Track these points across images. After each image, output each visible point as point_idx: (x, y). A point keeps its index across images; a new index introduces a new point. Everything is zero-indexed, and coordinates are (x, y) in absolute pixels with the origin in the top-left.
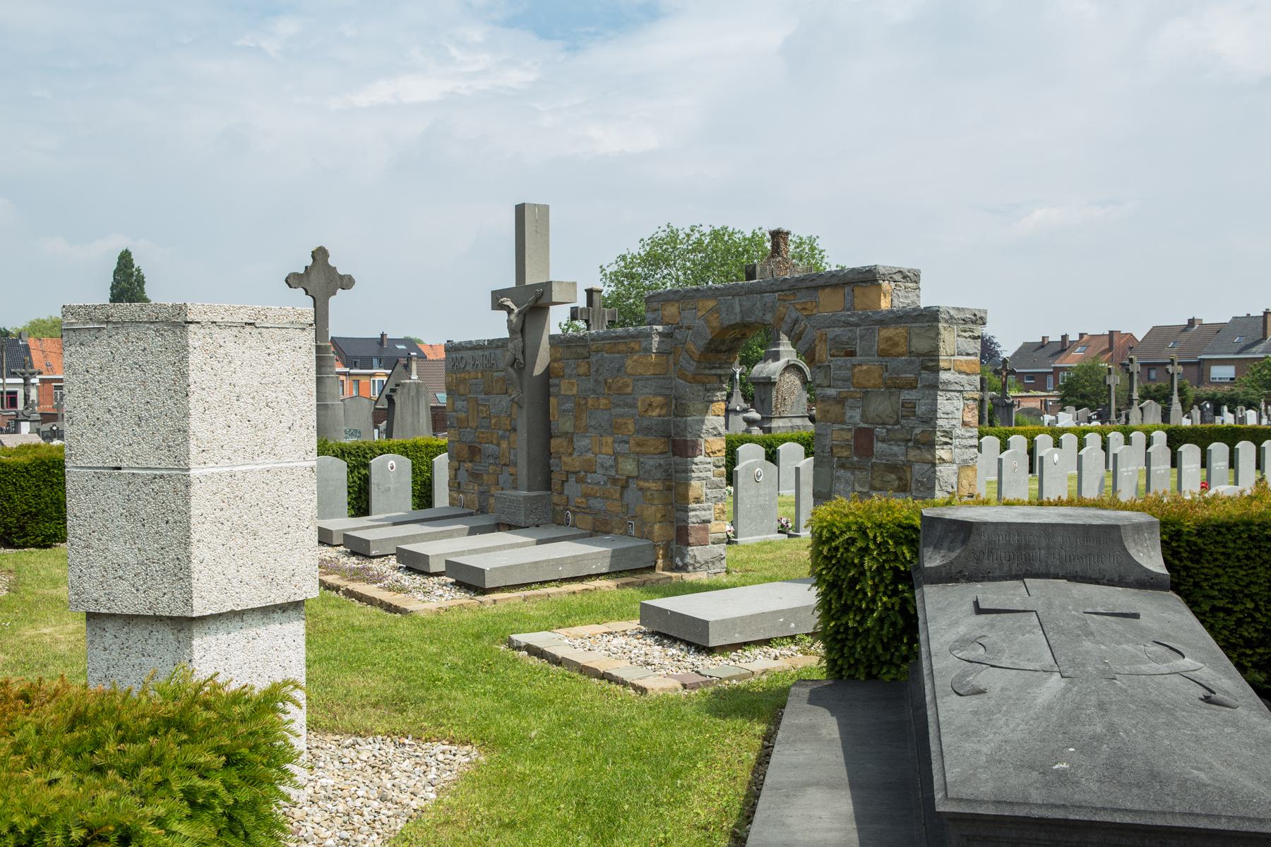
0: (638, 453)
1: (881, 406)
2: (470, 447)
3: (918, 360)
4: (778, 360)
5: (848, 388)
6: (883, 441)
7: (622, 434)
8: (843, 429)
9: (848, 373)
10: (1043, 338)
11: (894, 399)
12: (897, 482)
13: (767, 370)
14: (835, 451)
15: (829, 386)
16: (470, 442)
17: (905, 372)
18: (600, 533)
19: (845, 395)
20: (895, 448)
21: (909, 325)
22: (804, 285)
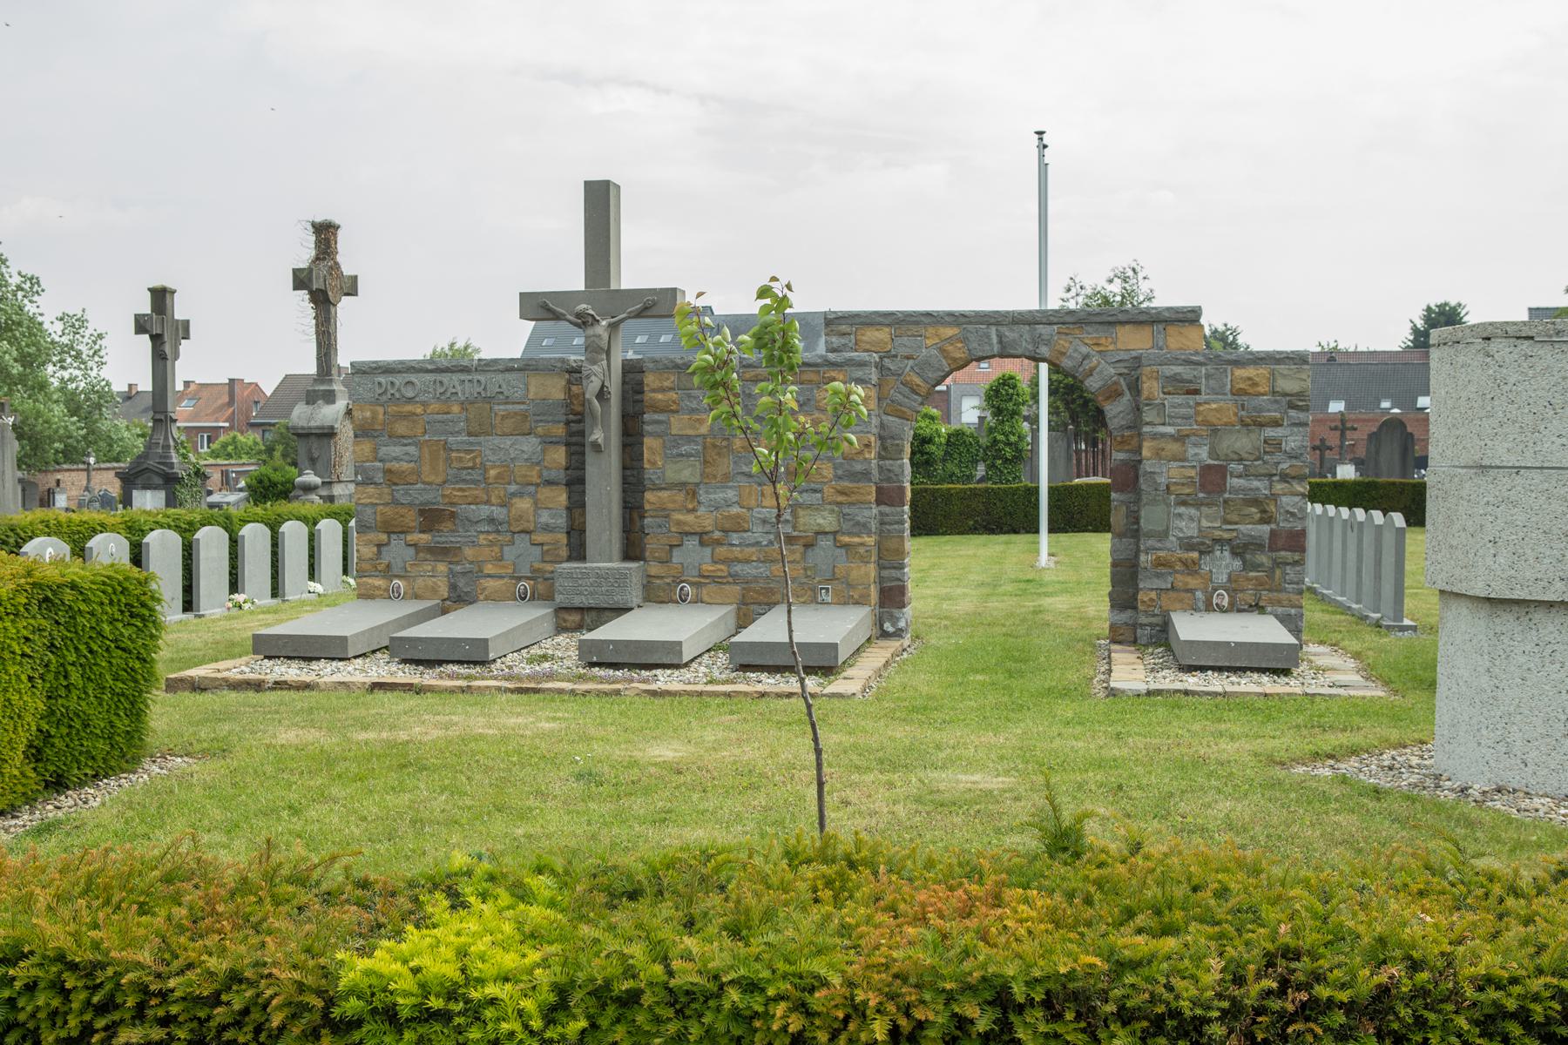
0: (839, 504)
1: (1243, 443)
2: (422, 512)
3: (1284, 400)
4: (333, 402)
6: (1239, 477)
9: (1191, 411)
10: (130, 386)
11: (1253, 436)
15: (1164, 424)
16: (421, 504)
17: (1269, 411)
18: (607, 613)
20: (1256, 484)
22: (1098, 319)
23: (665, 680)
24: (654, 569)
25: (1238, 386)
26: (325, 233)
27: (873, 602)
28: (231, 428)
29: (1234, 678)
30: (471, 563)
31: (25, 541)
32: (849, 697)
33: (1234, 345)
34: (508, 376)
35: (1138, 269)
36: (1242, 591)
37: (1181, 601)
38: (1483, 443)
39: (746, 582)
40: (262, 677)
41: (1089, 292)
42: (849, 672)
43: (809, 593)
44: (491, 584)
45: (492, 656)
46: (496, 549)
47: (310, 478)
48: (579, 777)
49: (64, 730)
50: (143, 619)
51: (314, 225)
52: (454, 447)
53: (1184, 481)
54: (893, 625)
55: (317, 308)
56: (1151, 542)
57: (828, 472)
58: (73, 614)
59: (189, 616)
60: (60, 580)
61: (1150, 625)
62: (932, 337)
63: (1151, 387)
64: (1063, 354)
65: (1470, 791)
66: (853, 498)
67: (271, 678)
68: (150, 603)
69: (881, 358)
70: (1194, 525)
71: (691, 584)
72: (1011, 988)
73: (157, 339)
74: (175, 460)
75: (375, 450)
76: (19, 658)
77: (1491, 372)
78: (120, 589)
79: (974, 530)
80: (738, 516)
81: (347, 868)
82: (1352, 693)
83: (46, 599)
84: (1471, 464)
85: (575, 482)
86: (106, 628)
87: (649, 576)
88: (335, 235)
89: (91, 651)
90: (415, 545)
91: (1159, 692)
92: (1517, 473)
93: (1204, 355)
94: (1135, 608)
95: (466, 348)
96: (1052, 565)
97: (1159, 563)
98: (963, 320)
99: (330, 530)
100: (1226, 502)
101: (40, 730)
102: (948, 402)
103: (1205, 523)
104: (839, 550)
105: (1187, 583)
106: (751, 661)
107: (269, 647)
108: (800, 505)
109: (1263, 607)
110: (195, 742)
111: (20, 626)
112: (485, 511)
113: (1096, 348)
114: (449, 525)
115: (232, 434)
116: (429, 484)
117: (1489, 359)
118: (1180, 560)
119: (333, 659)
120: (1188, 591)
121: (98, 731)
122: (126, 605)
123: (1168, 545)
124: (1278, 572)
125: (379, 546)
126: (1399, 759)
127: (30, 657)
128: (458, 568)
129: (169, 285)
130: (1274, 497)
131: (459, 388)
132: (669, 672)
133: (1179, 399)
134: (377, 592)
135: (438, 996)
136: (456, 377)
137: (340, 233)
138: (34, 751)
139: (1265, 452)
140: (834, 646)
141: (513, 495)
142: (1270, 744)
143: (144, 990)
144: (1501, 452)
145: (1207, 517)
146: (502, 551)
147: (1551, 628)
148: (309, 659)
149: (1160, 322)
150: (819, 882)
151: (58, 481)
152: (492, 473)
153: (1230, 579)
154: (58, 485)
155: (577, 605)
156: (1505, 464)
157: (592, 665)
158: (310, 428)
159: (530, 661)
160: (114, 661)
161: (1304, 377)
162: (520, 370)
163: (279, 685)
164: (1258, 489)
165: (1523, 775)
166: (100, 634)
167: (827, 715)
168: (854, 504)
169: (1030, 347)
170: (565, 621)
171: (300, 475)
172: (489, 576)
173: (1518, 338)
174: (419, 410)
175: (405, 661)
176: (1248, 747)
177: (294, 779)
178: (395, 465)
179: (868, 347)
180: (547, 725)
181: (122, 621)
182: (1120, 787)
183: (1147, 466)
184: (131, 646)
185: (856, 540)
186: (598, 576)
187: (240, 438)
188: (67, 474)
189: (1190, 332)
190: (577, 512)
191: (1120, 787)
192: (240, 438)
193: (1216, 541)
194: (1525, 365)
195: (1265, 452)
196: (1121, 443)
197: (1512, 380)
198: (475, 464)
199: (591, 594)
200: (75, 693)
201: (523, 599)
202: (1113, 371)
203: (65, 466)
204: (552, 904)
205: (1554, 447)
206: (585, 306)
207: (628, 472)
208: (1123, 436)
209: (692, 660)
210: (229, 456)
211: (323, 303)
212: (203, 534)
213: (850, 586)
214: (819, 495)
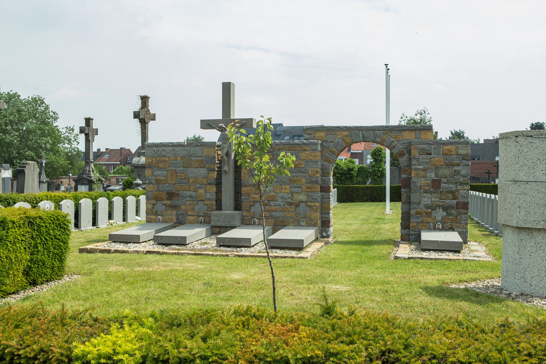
0: (307, 192)
1: (446, 172)
2: (168, 193)
5: (428, 165)
6: (445, 183)
7: (297, 184)
8: (426, 180)
9: (429, 161)
12: (452, 197)
15: (419, 165)
16: (167, 191)
17: (455, 161)
18: (229, 228)
19: (426, 168)
20: (451, 186)
21: (457, 145)
22: (397, 129)
23: (244, 251)
24: (245, 213)
25: (445, 152)
26: (145, 100)
27: (319, 225)
28: (121, 164)
29: (440, 254)
30: (184, 211)
31: (39, 202)
32: (305, 258)
33: (463, 137)
34: (197, 148)
35: (426, 111)
36: (446, 223)
37: (425, 226)
38: (515, 173)
39: (276, 218)
40: (110, 248)
41: (409, 118)
42: (308, 249)
43: (297, 222)
44: (190, 218)
45: (187, 242)
46: (192, 206)
47: (139, 181)
48: (205, 284)
49: (36, 266)
50: (65, 229)
51: (141, 97)
52: (179, 172)
53: (426, 185)
54: (326, 234)
55: (141, 125)
56: (414, 206)
57: (303, 181)
58: (39, 226)
59: (94, 227)
60: (36, 216)
61: (414, 234)
62: (340, 135)
63: (415, 153)
64: (385, 141)
65: (512, 295)
66: (312, 190)
67: (113, 249)
68: (67, 223)
69: (322, 142)
70: (430, 200)
71: (257, 219)
72: (290, 361)
73: (87, 135)
74: (92, 175)
75: (153, 173)
76: (20, 241)
77: (518, 148)
78: (56, 219)
79: (367, 201)
80: (273, 196)
81: (91, 314)
82: (480, 259)
83: (30, 222)
84: (511, 180)
85: (218, 183)
86: (51, 231)
87: (243, 216)
88: (148, 100)
89: (46, 239)
90: (165, 205)
91: (412, 258)
92: (527, 183)
93: (433, 141)
94: (409, 228)
95: (199, 137)
96: (391, 213)
97: (417, 213)
98: (350, 129)
99: (143, 198)
100: (441, 192)
101: (28, 265)
102: (362, 156)
103: (433, 199)
104: (307, 208)
105: (427, 220)
106: (274, 245)
107: (114, 239)
108: (294, 192)
109: (454, 229)
110: (82, 270)
111: (21, 231)
112: (188, 193)
113: (396, 139)
114: (176, 198)
115: (121, 166)
116: (170, 184)
117: (517, 144)
118: (425, 212)
119: (135, 243)
120: (427, 223)
121: (48, 266)
122: (58, 224)
123: (420, 207)
124: (459, 217)
125: (153, 205)
126: (490, 283)
127: (25, 241)
128: (179, 212)
129: (91, 117)
130: (458, 191)
131: (180, 152)
132: (246, 249)
133: (424, 156)
134: (153, 220)
135: (104, 358)
136: (179, 148)
137: (150, 100)
138: (26, 272)
139: (454, 175)
140: (302, 241)
141: (198, 188)
142: (445, 277)
143: (12, 353)
144: (522, 176)
145: (434, 197)
146: (194, 207)
147: (540, 238)
148: (127, 243)
149: (418, 130)
150: (240, 322)
151: (62, 182)
152: (191, 180)
153: (442, 219)
154: (62, 183)
155: (218, 225)
156: (523, 180)
157: (221, 246)
158: (139, 165)
159: (201, 244)
160: (54, 243)
161: (468, 149)
162: (200, 146)
163: (116, 251)
164: (452, 188)
165: (530, 289)
166: (49, 234)
167: (295, 264)
168: (312, 192)
169: (373, 138)
170: (214, 231)
171: (135, 180)
172: (190, 215)
173: (527, 136)
174: (167, 159)
175: (159, 244)
176: (437, 278)
177: (111, 283)
178: (159, 178)
179: (318, 138)
180: (199, 266)
181: (57, 229)
182: (387, 291)
183: (413, 180)
184: (60, 238)
185: (313, 204)
186: (226, 216)
187: (123, 167)
188: (64, 179)
189: (429, 133)
190: (219, 194)
191: (387, 291)
192: (123, 167)
193: (437, 206)
194: (530, 146)
195: (454, 175)
196: (404, 171)
197: (525, 151)
198: (185, 177)
199: (223, 222)
200: (40, 253)
201: (201, 223)
202: (402, 147)
203: (64, 177)
204: (151, 328)
205: (540, 174)
206: (222, 124)
207: (237, 181)
208: (405, 169)
209: (255, 245)
210: (120, 173)
211: (144, 123)
212: (99, 200)
213: (311, 220)
214: (301, 189)
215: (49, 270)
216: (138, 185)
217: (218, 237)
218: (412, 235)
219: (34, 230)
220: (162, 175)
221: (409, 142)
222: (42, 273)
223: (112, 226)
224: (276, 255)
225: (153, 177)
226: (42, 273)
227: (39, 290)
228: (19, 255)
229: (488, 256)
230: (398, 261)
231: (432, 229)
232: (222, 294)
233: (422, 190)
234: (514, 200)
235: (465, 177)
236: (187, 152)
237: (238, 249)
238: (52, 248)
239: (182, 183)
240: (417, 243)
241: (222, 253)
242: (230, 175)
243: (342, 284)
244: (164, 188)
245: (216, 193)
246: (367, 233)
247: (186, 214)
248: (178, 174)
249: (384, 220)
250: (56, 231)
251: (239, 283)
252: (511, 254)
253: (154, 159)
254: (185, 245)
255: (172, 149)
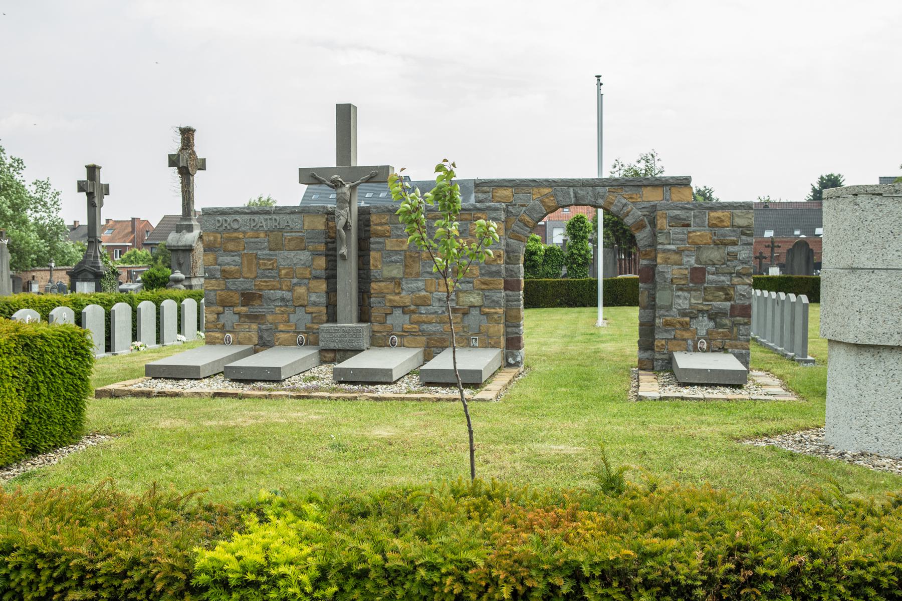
0: (482, 290)
1: (715, 254)
2: (243, 295)
3: (739, 230)
4: (192, 231)
6: (713, 274)
9: (686, 237)
10: (75, 222)
11: (721, 251)
13: (184, 239)
14: (674, 281)
15: (669, 244)
16: (242, 290)
17: (730, 236)
18: (350, 353)
20: (723, 278)
22: (632, 184)
23: (382, 391)
24: (376, 327)
26: (187, 134)
27: (502, 346)
28: (133, 246)
29: (710, 390)
31: (14, 311)
34: (292, 216)
35: (655, 155)
36: (715, 340)
37: (679, 346)
38: (853, 255)
39: (429, 335)
40: (151, 389)
41: (627, 168)
42: (488, 387)
44: (283, 336)
45: (283, 377)
46: (285, 316)
47: (179, 275)
49: (37, 420)
50: (83, 356)
51: (180, 129)
53: (681, 277)
54: (514, 360)
56: (662, 312)
58: (42, 353)
59: (109, 354)
60: (34, 334)
61: (662, 359)
63: (662, 223)
64: (612, 203)
66: (491, 287)
67: (156, 390)
68: (86, 347)
69: (507, 206)
70: (687, 302)
71: (398, 336)
73: (90, 195)
74: (100, 265)
75: (216, 259)
76: (11, 378)
77: (858, 214)
78: (69, 339)
79: (560, 305)
80: (425, 297)
81: (199, 499)
82: (778, 398)
83: (27, 345)
84: (846, 267)
85: (331, 277)
88: (193, 135)
89: (52, 375)
90: (239, 314)
91: (667, 398)
93: (693, 204)
94: (653, 350)
96: (605, 325)
97: (667, 324)
98: (553, 184)
100: (705, 288)
102: (545, 231)
103: (693, 301)
105: (683, 336)
106: (432, 380)
107: (154, 372)
109: (726, 349)
110: (112, 427)
111: (11, 360)
112: (279, 294)
113: (630, 200)
114: (258, 302)
115: (133, 250)
116: (247, 278)
117: (856, 207)
118: (679, 322)
119: (192, 379)
121: (56, 421)
122: (73, 348)
123: (672, 313)
124: (735, 329)
125: (218, 314)
126: (805, 436)
127: (17, 378)
128: (264, 327)
129: (97, 164)
131: (264, 223)
132: (385, 386)
133: (678, 230)
134: (217, 341)
135: (252, 573)
136: (262, 217)
137: (196, 134)
140: (480, 372)
141: (295, 284)
142: (730, 428)
144: (864, 260)
145: (694, 297)
146: (288, 317)
147: (892, 361)
148: (178, 379)
152: (283, 272)
153: (707, 333)
154: (33, 279)
155: (332, 348)
156: (866, 267)
157: (341, 382)
158: (178, 246)
159: (305, 380)
160: (65, 380)
162: (299, 213)
163: (161, 394)
164: (723, 281)
165: (876, 445)
169: (593, 200)
170: (325, 357)
171: (172, 273)
173: (873, 194)
174: (241, 236)
175: (233, 380)
178: (227, 268)
179: (499, 199)
181: (70, 357)
182: (644, 453)
183: (660, 268)
185: (493, 310)
186: (344, 331)
187: (138, 252)
188: (39, 273)
189: (685, 191)
190: (332, 294)
191: (644, 453)
192: (138, 252)
193: (700, 311)
194: (877, 210)
195: (728, 260)
197: (870, 219)
199: (340, 341)
201: (301, 344)
203: (37, 268)
204: (318, 520)
207: (361, 272)
208: (646, 251)
209: (398, 380)
210: (132, 262)
211: (186, 174)
213: (489, 337)
214: (471, 285)
215: (57, 428)
216: (178, 281)
217: (335, 367)
218: (657, 359)
219: (33, 358)
220: (233, 263)
221: (653, 206)
222: (47, 433)
223: (138, 352)
224: (437, 395)
225: (218, 267)
226: (47, 433)
227: (44, 463)
228: (8, 401)
229: (788, 393)
230: (644, 405)
231: (692, 349)
232: (367, 463)
233: (675, 286)
234: (851, 299)
235: (746, 263)
236: (276, 224)
237: (371, 387)
238: (62, 389)
239: (268, 277)
240: (667, 374)
241: (345, 395)
242: (351, 262)
243: (565, 442)
244: (236, 285)
245: (327, 293)
246: (580, 358)
247: (274, 330)
248: (261, 261)
249: (599, 337)
250: (69, 360)
251: (391, 444)
252: (843, 388)
253: (219, 236)
254: (278, 381)
255: (250, 219)
